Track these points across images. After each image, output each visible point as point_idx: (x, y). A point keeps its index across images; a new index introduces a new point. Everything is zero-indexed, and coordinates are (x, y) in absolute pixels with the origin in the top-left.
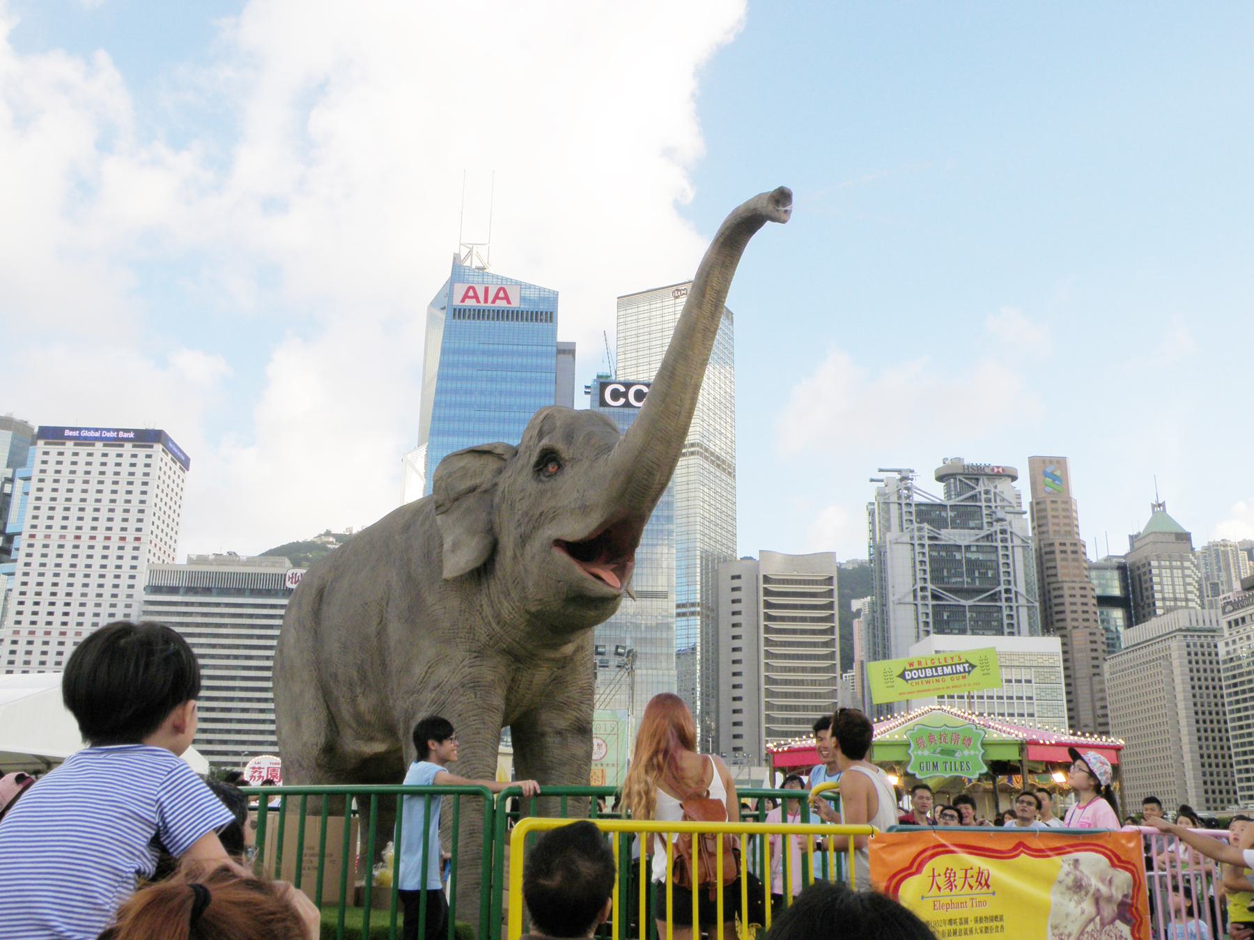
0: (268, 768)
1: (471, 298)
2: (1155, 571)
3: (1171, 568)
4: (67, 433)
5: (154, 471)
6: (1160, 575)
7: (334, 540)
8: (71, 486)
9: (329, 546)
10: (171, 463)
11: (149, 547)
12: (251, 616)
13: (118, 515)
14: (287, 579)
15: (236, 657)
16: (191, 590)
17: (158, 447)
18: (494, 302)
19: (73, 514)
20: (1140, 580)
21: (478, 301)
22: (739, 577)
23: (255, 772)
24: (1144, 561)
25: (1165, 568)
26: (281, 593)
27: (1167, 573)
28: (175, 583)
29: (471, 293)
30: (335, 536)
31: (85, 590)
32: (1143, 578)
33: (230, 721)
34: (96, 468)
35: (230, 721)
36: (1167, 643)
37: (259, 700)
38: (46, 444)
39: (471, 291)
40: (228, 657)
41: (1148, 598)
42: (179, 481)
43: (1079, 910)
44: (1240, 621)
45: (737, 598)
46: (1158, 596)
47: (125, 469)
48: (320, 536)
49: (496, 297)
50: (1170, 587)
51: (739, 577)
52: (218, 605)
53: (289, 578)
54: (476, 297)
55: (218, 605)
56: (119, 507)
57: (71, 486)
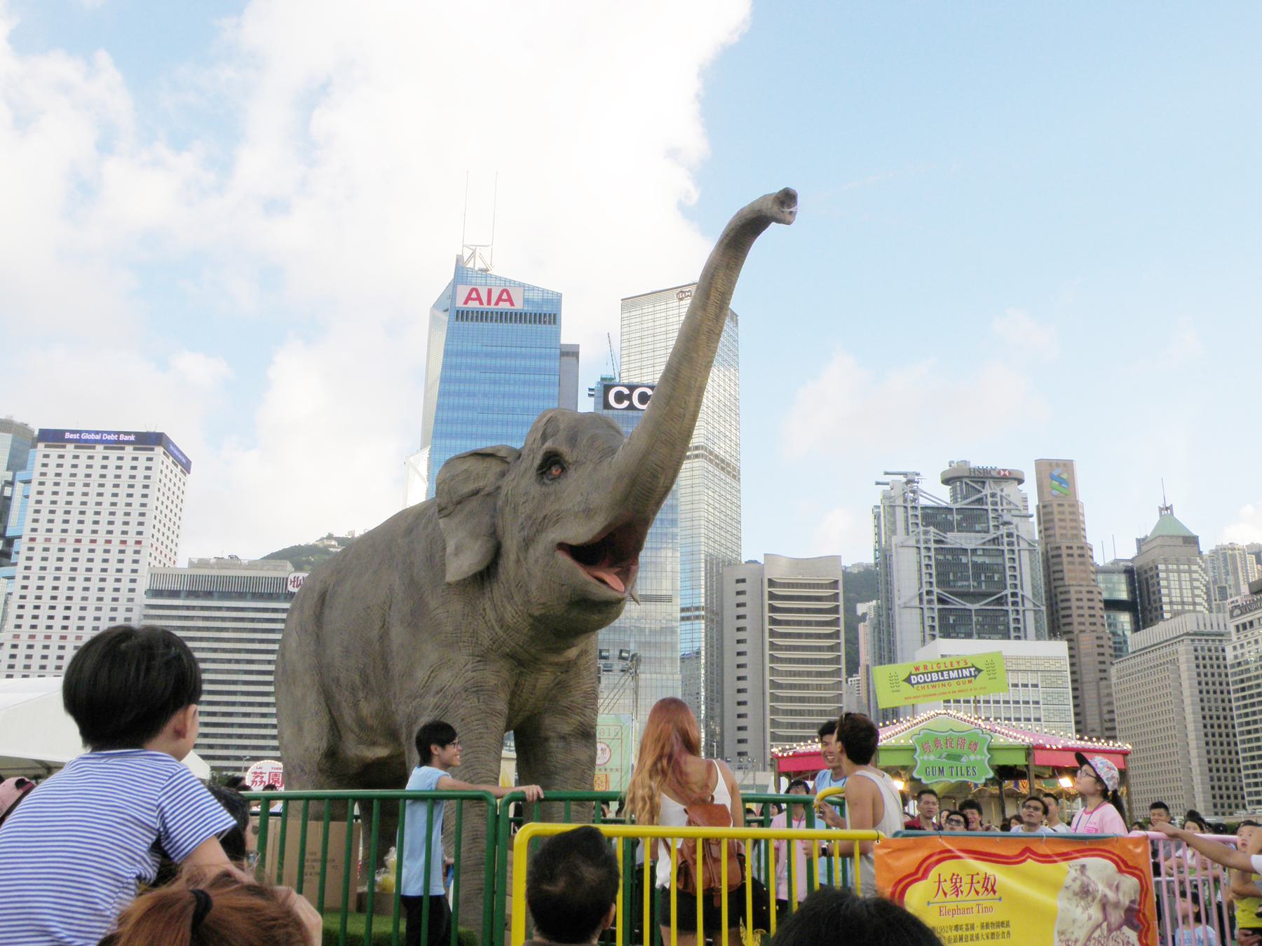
0: (270, 773)
1: (474, 299)
2: (1162, 575)
3: (1179, 571)
4: (68, 436)
5: (155, 474)
6: (1167, 579)
7: (336, 544)
8: (71, 489)
9: (331, 549)
10: (172, 466)
11: (150, 550)
12: (252, 620)
13: (119, 518)
14: (289, 583)
15: (238, 661)
16: (192, 594)
17: (159, 450)
18: (497, 304)
19: (74, 517)
20: (1147, 583)
21: (481, 303)
22: (743, 581)
23: (257, 777)
24: (1151, 565)
25: (1173, 571)
26: (282, 597)
27: (1174, 576)
28: (176, 587)
29: (474, 295)
30: (337, 539)
31: (86, 594)
32: (1150, 582)
33: (231, 725)
34: (97, 471)
35: (231, 725)
36: (1174, 647)
37: (261, 705)
38: (46, 446)
39: (474, 292)
40: (229, 661)
41: (1155, 602)
42: (181, 484)
43: (1086, 916)
44: (1248, 625)
45: (742, 601)
46: (1165, 599)
47: (126, 472)
48: (322, 539)
49: (500, 299)
50: (1178, 591)
51: (743, 581)
52: (219, 609)
53: (291, 582)
54: (479, 299)
55: (219, 609)
56: (120, 510)
57: (71, 489)
